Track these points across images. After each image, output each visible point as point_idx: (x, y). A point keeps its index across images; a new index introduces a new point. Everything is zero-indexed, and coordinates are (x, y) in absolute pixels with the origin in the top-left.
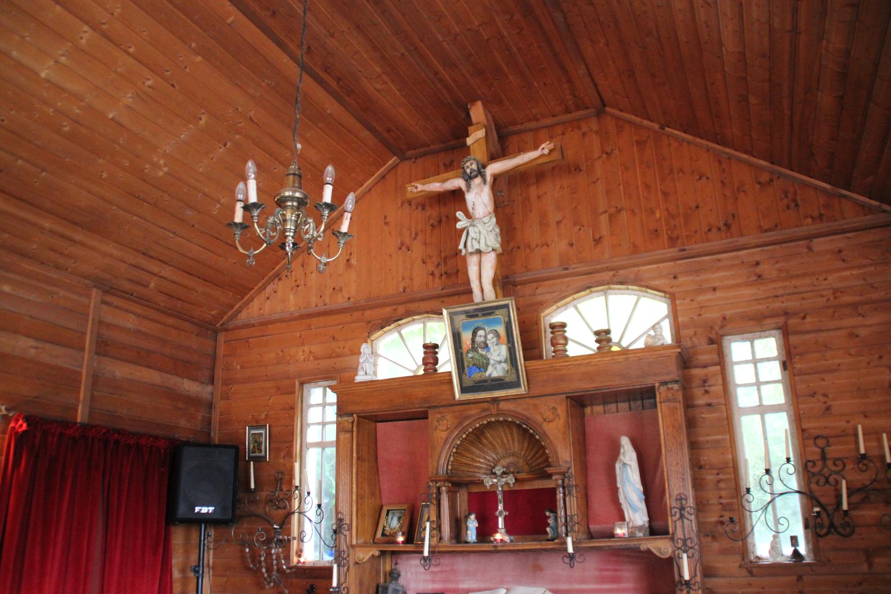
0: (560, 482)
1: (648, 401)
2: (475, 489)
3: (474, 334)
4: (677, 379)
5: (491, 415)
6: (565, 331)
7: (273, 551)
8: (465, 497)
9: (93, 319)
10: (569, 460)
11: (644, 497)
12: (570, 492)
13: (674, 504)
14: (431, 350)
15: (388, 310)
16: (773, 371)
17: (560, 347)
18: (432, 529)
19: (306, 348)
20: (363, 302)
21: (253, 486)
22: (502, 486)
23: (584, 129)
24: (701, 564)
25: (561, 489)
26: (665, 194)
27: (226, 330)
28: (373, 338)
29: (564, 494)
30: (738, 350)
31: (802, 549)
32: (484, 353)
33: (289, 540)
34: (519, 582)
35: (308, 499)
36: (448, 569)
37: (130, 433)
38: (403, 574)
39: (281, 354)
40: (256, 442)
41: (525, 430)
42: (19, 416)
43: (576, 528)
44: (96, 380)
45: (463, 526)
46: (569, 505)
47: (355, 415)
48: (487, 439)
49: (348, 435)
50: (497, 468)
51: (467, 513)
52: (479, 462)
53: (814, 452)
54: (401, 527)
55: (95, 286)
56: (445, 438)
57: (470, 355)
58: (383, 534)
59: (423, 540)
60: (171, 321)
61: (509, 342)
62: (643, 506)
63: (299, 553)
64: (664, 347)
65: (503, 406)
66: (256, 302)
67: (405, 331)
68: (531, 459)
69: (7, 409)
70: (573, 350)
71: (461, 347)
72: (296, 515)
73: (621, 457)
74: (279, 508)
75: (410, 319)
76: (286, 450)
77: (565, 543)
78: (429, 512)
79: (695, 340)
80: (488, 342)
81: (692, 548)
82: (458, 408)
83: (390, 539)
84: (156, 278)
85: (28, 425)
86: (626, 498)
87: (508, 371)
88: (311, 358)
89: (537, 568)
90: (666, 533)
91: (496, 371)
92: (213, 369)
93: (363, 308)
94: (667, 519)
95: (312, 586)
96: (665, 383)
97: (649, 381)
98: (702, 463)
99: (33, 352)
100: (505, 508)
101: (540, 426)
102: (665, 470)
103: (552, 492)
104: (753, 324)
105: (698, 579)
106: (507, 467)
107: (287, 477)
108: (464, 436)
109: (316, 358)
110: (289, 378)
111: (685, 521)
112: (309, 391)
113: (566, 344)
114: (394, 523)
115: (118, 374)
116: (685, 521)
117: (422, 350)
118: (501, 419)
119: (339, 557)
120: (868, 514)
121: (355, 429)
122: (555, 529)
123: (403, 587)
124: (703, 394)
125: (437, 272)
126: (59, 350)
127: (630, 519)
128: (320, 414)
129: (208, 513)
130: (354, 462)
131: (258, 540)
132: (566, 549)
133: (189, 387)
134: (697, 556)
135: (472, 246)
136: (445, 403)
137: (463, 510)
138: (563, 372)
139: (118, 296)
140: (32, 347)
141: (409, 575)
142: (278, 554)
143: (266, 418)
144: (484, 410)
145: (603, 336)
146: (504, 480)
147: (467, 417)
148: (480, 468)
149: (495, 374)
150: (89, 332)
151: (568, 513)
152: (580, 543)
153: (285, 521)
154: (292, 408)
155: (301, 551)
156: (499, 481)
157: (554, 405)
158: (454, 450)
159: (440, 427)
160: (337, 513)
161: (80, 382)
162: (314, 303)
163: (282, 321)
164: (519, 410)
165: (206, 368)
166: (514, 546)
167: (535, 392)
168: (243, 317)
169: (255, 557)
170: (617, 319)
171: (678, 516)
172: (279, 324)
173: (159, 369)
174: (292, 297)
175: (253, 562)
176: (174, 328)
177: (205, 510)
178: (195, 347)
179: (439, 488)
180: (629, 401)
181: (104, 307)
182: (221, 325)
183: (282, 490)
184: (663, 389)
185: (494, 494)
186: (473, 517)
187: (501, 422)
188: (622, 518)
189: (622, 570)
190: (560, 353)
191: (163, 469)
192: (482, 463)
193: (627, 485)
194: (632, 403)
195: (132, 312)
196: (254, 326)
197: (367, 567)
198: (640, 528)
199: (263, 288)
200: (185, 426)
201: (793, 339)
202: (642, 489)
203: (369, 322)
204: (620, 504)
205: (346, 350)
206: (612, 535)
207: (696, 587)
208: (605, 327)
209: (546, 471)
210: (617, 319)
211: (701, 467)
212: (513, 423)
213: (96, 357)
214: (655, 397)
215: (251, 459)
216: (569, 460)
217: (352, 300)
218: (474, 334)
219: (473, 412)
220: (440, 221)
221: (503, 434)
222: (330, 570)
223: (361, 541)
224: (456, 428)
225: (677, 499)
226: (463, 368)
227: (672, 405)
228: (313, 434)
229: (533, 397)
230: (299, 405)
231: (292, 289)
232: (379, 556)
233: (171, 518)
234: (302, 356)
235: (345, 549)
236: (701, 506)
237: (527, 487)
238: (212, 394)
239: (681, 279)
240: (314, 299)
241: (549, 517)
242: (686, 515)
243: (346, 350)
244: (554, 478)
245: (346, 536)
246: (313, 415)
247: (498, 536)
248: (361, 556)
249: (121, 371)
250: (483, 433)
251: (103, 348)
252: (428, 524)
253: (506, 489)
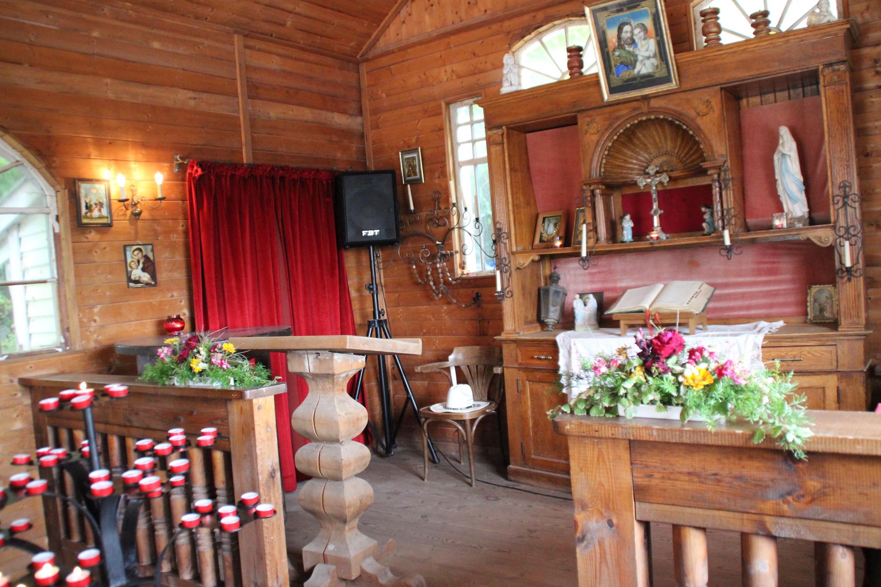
0: (716, 176)
1: (809, 88)
2: (629, 191)
3: (620, 30)
4: (845, 58)
5: (642, 114)
6: (718, 18)
7: (438, 266)
8: (620, 200)
9: (240, 65)
10: (724, 153)
11: (803, 188)
12: (726, 186)
13: (837, 192)
14: (576, 53)
15: (526, 18)
17: (712, 36)
18: (588, 231)
19: (448, 68)
20: (500, 14)
21: (412, 208)
22: (656, 186)
24: (864, 253)
25: (717, 184)
27: (367, 60)
28: (514, 49)
29: (720, 188)
32: (631, 49)
33: (452, 255)
34: (675, 278)
35: (466, 215)
36: (605, 269)
37: (292, 168)
38: (562, 277)
39: (423, 77)
40: (410, 165)
41: (679, 127)
42: (193, 162)
43: (733, 221)
44: (253, 122)
45: (619, 227)
46: (725, 199)
47: (504, 127)
48: (639, 139)
49: (499, 148)
50: (651, 167)
51: (622, 214)
52: (632, 163)
54: (557, 233)
55: (236, 32)
56: (595, 141)
57: (617, 53)
58: (541, 241)
59: (580, 243)
60: (312, 57)
61: (657, 35)
62: (803, 197)
63: (463, 267)
64: (830, 25)
65: (654, 103)
66: (392, 30)
67: (546, 38)
68: (685, 156)
69: (181, 158)
70: (726, 39)
71: (606, 46)
72: (456, 230)
73: (780, 148)
74: (439, 225)
75: (550, 25)
76: (440, 170)
77: (722, 237)
78: (584, 215)
79: (867, 16)
80: (635, 37)
81: (854, 236)
82: (608, 109)
83: (549, 243)
84: (291, 16)
85: (203, 170)
86: (784, 189)
87: (657, 67)
88: (454, 77)
89: (694, 264)
90: (828, 221)
91: (644, 68)
92: (359, 101)
93: (500, 20)
94: (829, 210)
95: (477, 294)
96: (830, 65)
97: (812, 64)
98: (869, 150)
99: (192, 103)
100: (660, 207)
101: (693, 120)
102: (828, 157)
103: (709, 188)
105: (860, 266)
106: (661, 166)
107: (444, 196)
108: (615, 137)
109: (459, 77)
110: (434, 100)
111: (849, 209)
112: (456, 111)
113: (719, 32)
114: (551, 230)
115: (273, 115)
116: (849, 209)
117: (566, 54)
118: (653, 117)
119: (500, 264)
121: (505, 140)
122: (712, 224)
123: (563, 288)
124: (874, 76)
126: (213, 99)
127: (788, 209)
128: (469, 132)
129: (374, 235)
130: (508, 173)
131: (423, 257)
132: (723, 242)
133: (340, 120)
134: (859, 244)
136: (594, 105)
137: (617, 212)
138: (716, 62)
139: (258, 39)
140: (191, 98)
141: (568, 278)
142: (443, 268)
143: (417, 141)
144: (635, 109)
145: (761, 19)
146: (658, 179)
147: (617, 118)
148: (632, 169)
150: (238, 77)
151: (725, 207)
152: (737, 235)
153: (447, 236)
154: (441, 129)
155: (464, 263)
156: (652, 180)
157: (707, 98)
158: (606, 153)
159: (591, 131)
160: (495, 223)
161: (240, 126)
162: (451, 20)
163: (421, 43)
164: (671, 106)
165: (352, 100)
166: (670, 242)
167: (686, 86)
168: (382, 45)
169: (422, 272)
171: (840, 204)
172: (418, 47)
173: (309, 106)
174: (427, 17)
175: (421, 277)
176: (316, 64)
177: (371, 233)
178: (339, 80)
179: (593, 192)
180: (789, 89)
181: (248, 51)
182: (363, 55)
183: (440, 209)
184: (827, 71)
185: (648, 195)
186: (628, 217)
187: (652, 120)
188: (780, 208)
189: (779, 262)
190: (714, 43)
191: (328, 199)
192: (635, 164)
193: (787, 176)
194: (791, 91)
195: (275, 54)
196: (393, 52)
197: (528, 271)
198: (799, 219)
199: (397, 12)
200: (341, 158)
202: (802, 179)
203: (509, 33)
204: (779, 196)
205: (489, 65)
206: (770, 227)
207: (858, 274)
208: (762, 9)
209: (701, 167)
211: (867, 155)
212: (664, 120)
213: (249, 101)
214: (817, 83)
215: (407, 182)
216: (724, 153)
217: (489, 12)
218: (620, 30)
219: (623, 113)
221: (655, 133)
222: (493, 278)
223: (520, 249)
224: (606, 130)
225: (840, 187)
226: (610, 67)
227: (837, 88)
228: (464, 153)
229: (685, 91)
230: (448, 126)
231: (426, 9)
232: (538, 261)
233: (341, 244)
234: (444, 76)
235: (506, 256)
236: (866, 195)
237: (681, 185)
238: (362, 124)
240: (450, 17)
241: (705, 213)
242: (850, 202)
243: (489, 65)
244: (709, 173)
245: (505, 244)
246: (462, 134)
247: (654, 235)
248: (522, 262)
249: (275, 112)
250: (634, 133)
251: (254, 91)
252: (584, 227)
253: (660, 188)
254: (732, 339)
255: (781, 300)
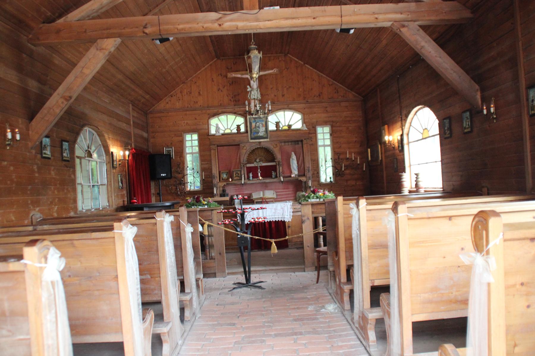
16: (328, 136)
19: (186, 122)
23: (280, 59)
26: (303, 84)
30: (319, 130)
31: (332, 180)
53: (337, 157)
62: (297, 169)
91: (261, 134)
104: (324, 123)
120: (347, 172)
125: (232, 100)
135: (252, 97)
149: (261, 135)
170: (290, 119)
177: (164, 175)
201: (334, 128)
210: (290, 119)
220: (232, 83)
239: (306, 110)
243: (201, 123)
254: (286, 204)
255: (290, 196)
